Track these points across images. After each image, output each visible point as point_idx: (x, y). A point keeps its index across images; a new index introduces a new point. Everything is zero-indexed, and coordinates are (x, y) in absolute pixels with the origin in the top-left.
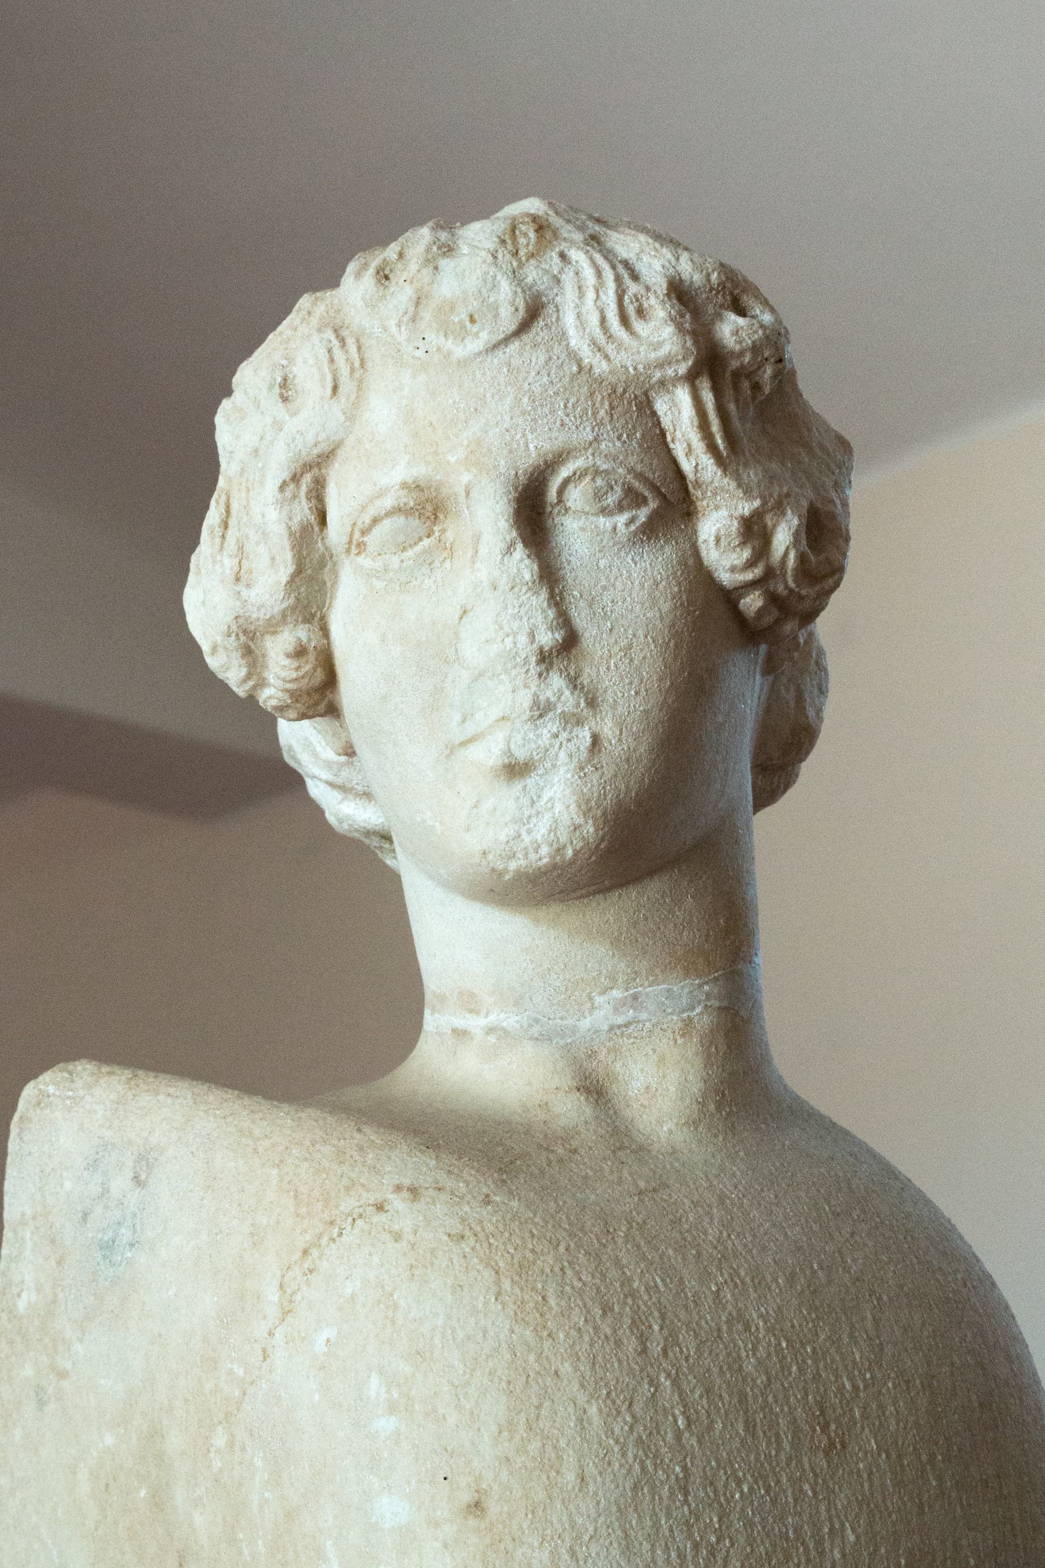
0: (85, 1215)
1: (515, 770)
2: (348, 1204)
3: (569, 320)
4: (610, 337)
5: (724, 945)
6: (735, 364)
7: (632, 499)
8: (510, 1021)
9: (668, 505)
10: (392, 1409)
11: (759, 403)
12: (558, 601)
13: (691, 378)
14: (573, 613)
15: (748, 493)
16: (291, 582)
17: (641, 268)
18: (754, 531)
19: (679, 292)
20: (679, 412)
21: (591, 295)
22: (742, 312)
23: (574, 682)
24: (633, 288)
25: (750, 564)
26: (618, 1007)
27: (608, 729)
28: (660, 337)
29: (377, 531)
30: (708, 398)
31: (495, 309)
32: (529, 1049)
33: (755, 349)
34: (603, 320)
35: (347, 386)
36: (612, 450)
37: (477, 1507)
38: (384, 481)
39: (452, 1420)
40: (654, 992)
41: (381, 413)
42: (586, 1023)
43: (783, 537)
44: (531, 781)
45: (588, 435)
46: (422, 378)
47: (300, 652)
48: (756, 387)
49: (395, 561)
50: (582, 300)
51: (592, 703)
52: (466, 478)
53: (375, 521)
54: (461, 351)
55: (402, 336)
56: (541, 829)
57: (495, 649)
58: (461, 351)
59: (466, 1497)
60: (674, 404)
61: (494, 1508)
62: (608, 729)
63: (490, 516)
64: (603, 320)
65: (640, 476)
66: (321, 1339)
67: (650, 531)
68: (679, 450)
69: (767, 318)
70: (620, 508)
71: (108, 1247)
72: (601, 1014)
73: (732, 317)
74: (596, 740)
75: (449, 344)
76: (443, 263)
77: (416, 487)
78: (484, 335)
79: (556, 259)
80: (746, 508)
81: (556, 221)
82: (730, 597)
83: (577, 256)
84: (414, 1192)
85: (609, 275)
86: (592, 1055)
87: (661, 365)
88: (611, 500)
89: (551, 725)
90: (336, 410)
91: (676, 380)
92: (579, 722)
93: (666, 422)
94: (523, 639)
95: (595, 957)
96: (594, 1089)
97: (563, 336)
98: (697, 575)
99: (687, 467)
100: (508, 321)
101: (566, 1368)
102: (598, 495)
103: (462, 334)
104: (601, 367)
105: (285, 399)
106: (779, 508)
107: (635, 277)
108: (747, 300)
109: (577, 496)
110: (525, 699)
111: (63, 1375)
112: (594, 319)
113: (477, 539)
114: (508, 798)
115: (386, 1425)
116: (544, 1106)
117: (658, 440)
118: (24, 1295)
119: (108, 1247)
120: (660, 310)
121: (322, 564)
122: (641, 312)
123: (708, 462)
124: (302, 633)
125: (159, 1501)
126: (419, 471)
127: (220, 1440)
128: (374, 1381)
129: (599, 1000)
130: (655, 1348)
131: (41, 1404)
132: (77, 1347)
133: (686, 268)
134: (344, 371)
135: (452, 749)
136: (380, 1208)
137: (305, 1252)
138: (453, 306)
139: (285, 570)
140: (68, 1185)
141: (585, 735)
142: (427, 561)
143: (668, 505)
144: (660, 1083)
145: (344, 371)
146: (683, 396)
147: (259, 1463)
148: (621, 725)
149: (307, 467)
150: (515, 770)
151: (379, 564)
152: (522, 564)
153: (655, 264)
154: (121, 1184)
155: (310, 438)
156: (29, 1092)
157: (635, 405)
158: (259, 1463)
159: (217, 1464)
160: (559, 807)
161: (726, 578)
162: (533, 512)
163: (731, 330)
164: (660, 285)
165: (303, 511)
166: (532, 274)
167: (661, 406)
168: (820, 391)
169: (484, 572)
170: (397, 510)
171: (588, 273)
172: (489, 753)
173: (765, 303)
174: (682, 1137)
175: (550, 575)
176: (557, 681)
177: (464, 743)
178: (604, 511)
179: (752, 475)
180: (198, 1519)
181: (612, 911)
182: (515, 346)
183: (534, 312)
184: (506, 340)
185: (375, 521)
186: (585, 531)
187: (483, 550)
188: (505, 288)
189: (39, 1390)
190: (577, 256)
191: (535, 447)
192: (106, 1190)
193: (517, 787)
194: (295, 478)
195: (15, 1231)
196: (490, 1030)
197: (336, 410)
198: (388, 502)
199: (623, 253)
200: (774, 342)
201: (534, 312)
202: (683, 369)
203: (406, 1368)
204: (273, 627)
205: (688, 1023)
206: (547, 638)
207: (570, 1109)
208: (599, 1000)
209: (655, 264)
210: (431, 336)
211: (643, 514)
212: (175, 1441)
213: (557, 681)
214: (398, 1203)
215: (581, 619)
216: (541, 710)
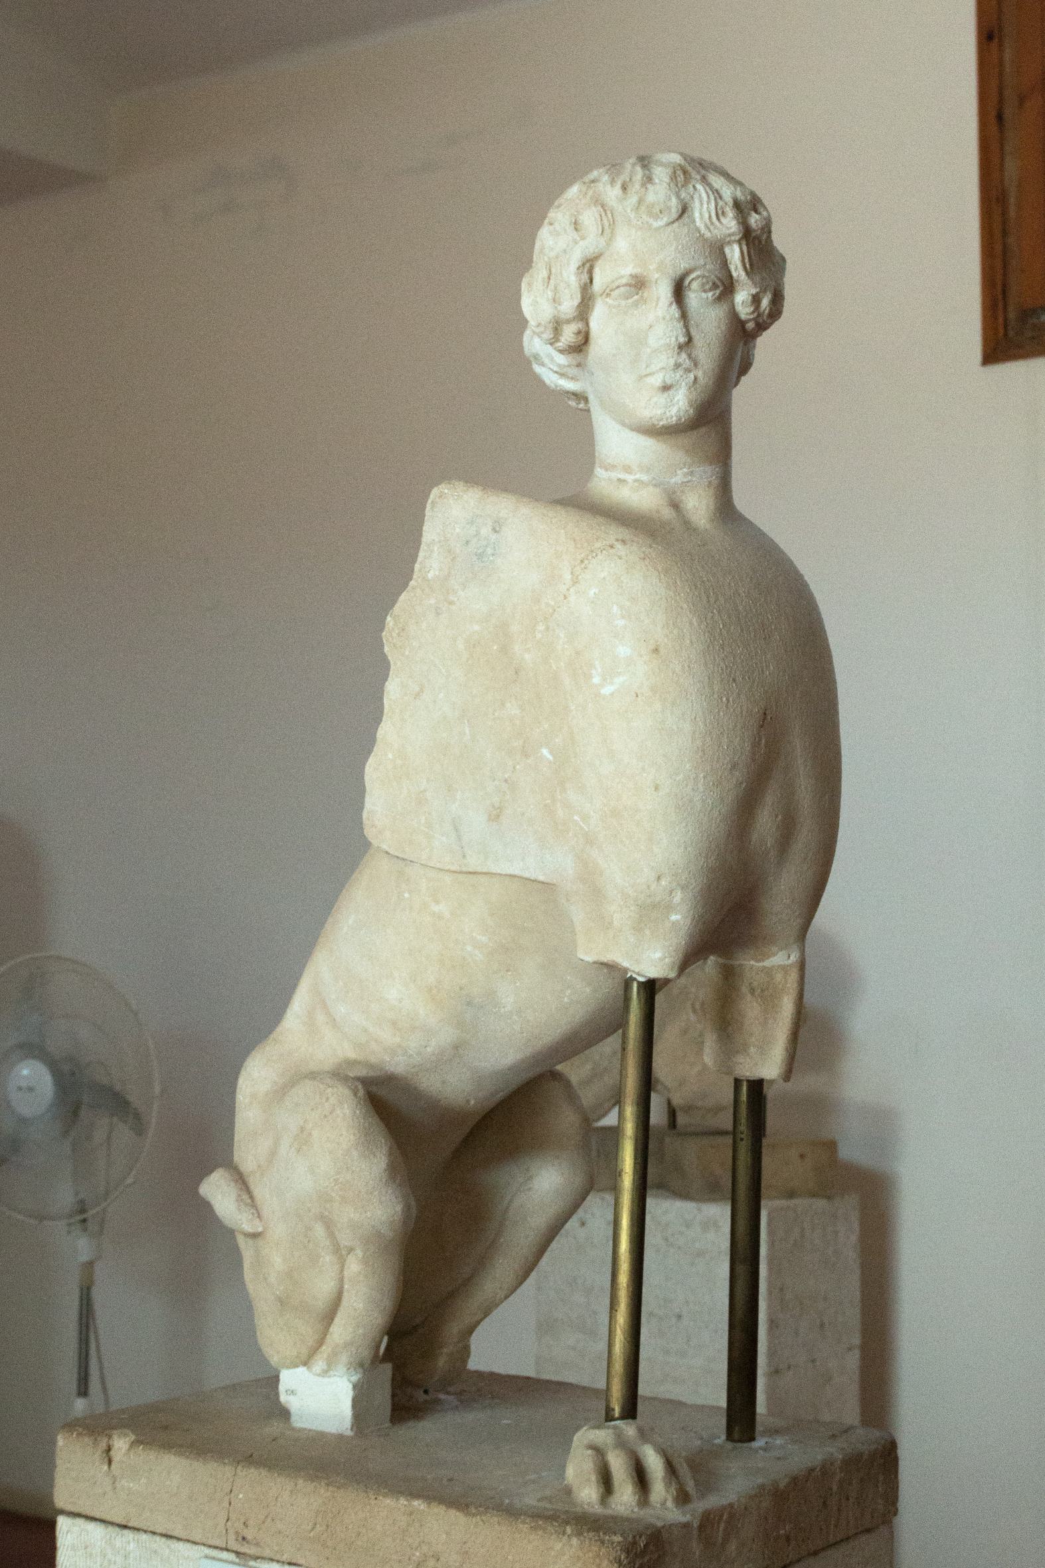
0: (467, 542)
1: (666, 388)
2: (598, 545)
3: (697, 215)
4: (712, 223)
5: (722, 455)
6: (754, 234)
7: (715, 286)
8: (644, 477)
9: (726, 287)
10: (623, 617)
11: (762, 252)
12: (686, 326)
13: (739, 242)
14: (692, 330)
15: (755, 284)
16: (578, 306)
17: (724, 195)
18: (756, 300)
19: (737, 205)
20: (734, 254)
21: (705, 206)
22: (756, 211)
23: (689, 356)
24: (721, 203)
25: (753, 312)
26: (685, 475)
27: (700, 374)
28: (730, 224)
29: (617, 292)
30: (745, 248)
31: (669, 208)
32: (651, 489)
33: (762, 229)
34: (710, 217)
35: (608, 231)
36: (712, 268)
37: (656, 651)
38: (623, 273)
39: (646, 622)
40: (699, 470)
41: (622, 244)
42: (673, 480)
43: (765, 302)
44: (671, 392)
45: (702, 262)
46: (639, 233)
47: (579, 332)
48: (760, 242)
49: (623, 303)
50: (702, 209)
51: (696, 365)
52: (657, 276)
53: (618, 287)
54: (656, 224)
55: (632, 215)
56: (674, 411)
57: (662, 342)
58: (656, 224)
59: (653, 647)
60: (732, 250)
61: (662, 651)
62: (700, 374)
63: (664, 291)
64: (710, 217)
65: (719, 279)
66: (592, 593)
67: (719, 299)
68: (732, 268)
69: (765, 213)
70: (710, 290)
71: (480, 556)
72: (679, 478)
73: (754, 214)
74: (696, 378)
75: (651, 221)
76: (649, 186)
77: (633, 276)
78: (665, 219)
79: (692, 189)
80: (754, 291)
81: (689, 168)
82: (742, 323)
83: (699, 186)
84: (624, 542)
85: (712, 197)
86: (674, 492)
87: (730, 235)
88: (707, 287)
89: (680, 372)
90: (602, 242)
91: (734, 241)
92: (690, 371)
93: (729, 256)
94: (673, 339)
95: (680, 456)
96: (675, 506)
97: (694, 221)
98: (734, 315)
99: (735, 274)
100: (674, 213)
101: (685, 606)
102: (703, 285)
103: (656, 218)
104: (708, 235)
105: (576, 229)
106: (765, 291)
107: (721, 198)
108: (759, 206)
109: (695, 285)
110: (672, 362)
111: (451, 603)
112: (707, 216)
113: (658, 299)
114: (662, 399)
115: (621, 623)
116: (658, 512)
117: (725, 264)
118: (432, 572)
119: (480, 556)
120: (730, 213)
121: (590, 298)
122: (723, 213)
123: (743, 273)
124: (580, 325)
125: (504, 649)
126: (637, 271)
127: (541, 627)
128: (615, 608)
129: (679, 472)
130: (712, 600)
131: (438, 614)
132: (461, 593)
133: (739, 194)
134: (606, 224)
135: (641, 378)
136: (612, 547)
137: (582, 561)
138: (653, 205)
139: (577, 301)
140: (458, 530)
141: (692, 376)
142: (636, 305)
143: (726, 287)
144: (699, 505)
145: (606, 224)
146: (736, 248)
147: (562, 635)
148: (704, 373)
149: (588, 261)
150: (666, 388)
151: (616, 303)
152: (675, 311)
153: (728, 192)
154: (485, 531)
155: (591, 250)
156: (435, 492)
157: (717, 250)
158: (562, 635)
159: (539, 636)
160: (681, 403)
161: (743, 317)
162: (679, 291)
163: (754, 220)
164: (731, 203)
165: (585, 277)
166: (683, 195)
167: (727, 250)
168: (779, 241)
169: (660, 312)
170: (626, 285)
171: (704, 195)
172: (657, 380)
173: (765, 208)
174: (708, 526)
175: (684, 316)
176: (684, 355)
177: (646, 376)
178: (705, 291)
179: (757, 278)
180: (527, 656)
181: (687, 440)
182: (676, 224)
183: (684, 210)
184: (673, 222)
185: (618, 287)
186: (696, 298)
187: (660, 304)
188: (674, 200)
189: (437, 608)
190: (699, 186)
191: (684, 265)
192: (478, 534)
193: (666, 395)
194: (584, 265)
195: (428, 546)
196: (636, 481)
197: (602, 242)
198: (624, 281)
199: (716, 186)
200: (767, 228)
201: (684, 210)
202: (737, 238)
203: (628, 604)
204: (568, 322)
205: (710, 482)
206: (682, 339)
207: (667, 513)
208: (679, 472)
209: (728, 192)
210: (644, 217)
211: (718, 292)
212: (515, 628)
213: (684, 355)
214: (619, 546)
215: (693, 332)
216: (677, 366)
